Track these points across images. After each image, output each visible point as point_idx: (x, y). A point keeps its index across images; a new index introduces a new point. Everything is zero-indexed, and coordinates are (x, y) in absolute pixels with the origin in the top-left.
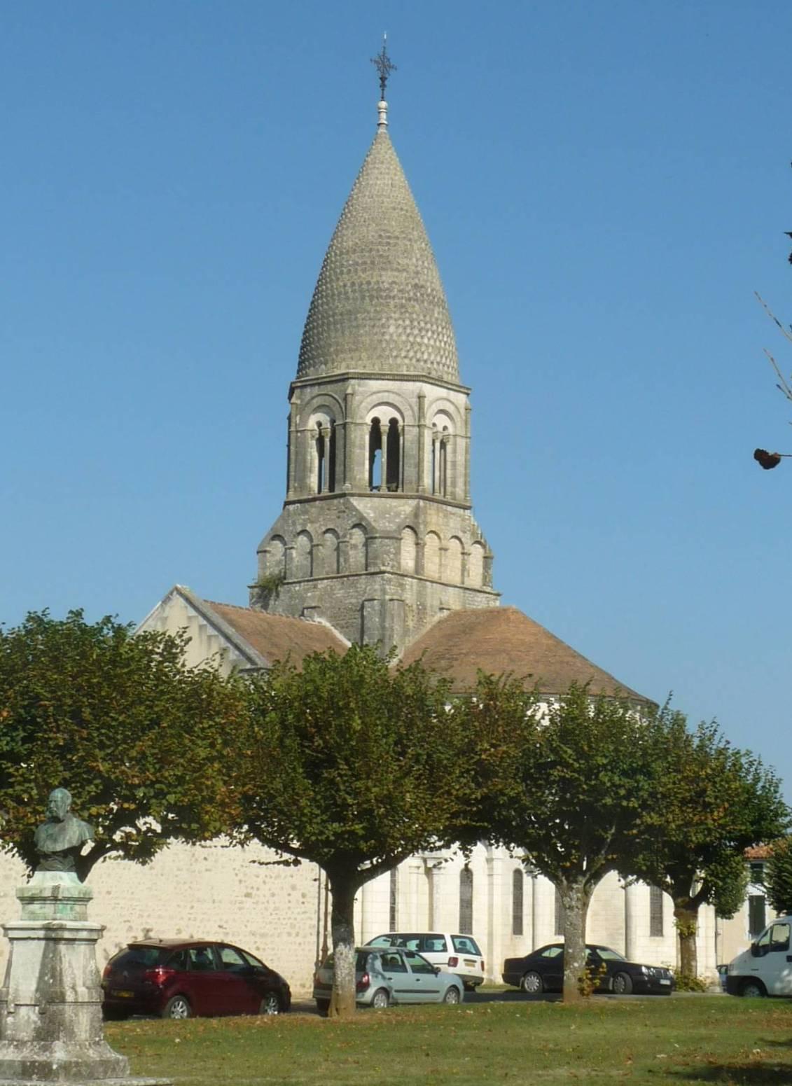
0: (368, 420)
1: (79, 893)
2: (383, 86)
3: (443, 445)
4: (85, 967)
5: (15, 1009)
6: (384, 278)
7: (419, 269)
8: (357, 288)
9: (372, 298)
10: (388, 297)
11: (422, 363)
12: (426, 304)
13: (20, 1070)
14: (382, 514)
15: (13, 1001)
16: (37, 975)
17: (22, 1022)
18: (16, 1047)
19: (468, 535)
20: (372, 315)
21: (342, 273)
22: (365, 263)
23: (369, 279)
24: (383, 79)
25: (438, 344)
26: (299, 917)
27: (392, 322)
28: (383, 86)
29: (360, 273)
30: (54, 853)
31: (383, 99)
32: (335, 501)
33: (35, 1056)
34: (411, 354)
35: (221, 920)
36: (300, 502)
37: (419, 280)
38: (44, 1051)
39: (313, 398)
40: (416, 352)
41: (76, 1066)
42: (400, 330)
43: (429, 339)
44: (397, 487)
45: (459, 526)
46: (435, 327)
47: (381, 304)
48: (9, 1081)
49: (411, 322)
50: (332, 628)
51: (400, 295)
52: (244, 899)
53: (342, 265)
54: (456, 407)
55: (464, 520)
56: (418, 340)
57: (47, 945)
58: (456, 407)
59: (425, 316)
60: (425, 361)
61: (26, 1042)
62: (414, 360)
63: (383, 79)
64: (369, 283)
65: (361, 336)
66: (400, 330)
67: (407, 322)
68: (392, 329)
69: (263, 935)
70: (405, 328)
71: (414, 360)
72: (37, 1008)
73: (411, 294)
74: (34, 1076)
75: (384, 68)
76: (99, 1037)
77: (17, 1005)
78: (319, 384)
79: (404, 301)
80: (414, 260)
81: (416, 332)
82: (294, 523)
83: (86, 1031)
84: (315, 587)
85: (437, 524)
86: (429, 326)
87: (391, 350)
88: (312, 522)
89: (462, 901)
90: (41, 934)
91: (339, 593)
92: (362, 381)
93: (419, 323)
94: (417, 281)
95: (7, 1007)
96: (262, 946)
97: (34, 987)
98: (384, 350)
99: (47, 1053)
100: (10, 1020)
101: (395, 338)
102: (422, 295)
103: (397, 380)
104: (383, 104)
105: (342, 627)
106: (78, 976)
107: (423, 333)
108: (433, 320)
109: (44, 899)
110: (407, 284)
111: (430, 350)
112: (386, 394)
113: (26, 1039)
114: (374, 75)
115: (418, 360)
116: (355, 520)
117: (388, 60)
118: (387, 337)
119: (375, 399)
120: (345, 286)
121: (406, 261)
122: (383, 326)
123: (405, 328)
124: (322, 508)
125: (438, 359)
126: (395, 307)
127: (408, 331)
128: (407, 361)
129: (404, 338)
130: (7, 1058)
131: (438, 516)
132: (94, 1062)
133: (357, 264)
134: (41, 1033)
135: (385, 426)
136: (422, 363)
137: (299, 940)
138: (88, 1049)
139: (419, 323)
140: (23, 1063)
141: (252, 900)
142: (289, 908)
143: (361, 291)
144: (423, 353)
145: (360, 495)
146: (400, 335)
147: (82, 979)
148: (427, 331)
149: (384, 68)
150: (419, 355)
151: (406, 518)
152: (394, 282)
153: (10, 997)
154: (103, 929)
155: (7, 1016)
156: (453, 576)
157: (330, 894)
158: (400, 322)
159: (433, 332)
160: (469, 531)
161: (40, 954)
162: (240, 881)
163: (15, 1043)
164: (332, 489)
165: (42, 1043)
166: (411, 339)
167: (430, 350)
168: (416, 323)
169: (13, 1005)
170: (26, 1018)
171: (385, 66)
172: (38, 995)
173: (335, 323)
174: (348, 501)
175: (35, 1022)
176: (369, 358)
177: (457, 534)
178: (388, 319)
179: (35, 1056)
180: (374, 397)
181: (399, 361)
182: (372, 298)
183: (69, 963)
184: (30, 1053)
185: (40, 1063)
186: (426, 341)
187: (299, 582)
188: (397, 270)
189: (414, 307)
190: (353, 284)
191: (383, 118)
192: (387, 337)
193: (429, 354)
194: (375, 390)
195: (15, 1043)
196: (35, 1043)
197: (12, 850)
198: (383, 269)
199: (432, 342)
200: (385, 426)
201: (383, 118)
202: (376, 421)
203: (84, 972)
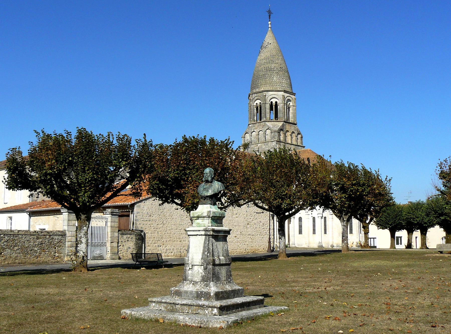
0: (255, 104)
1: (219, 214)
2: (270, 18)
3: (289, 108)
4: (223, 248)
5: (192, 267)
8: (265, 68)
9: (269, 71)
10: (273, 70)
13: (196, 295)
14: (274, 126)
15: (191, 264)
16: (202, 252)
17: (196, 273)
18: (193, 284)
19: (296, 131)
20: (269, 75)
21: (261, 65)
22: (267, 62)
23: (268, 66)
24: (270, 16)
26: (262, 230)
27: (275, 77)
28: (270, 18)
29: (266, 65)
30: (207, 196)
31: (270, 21)
32: (262, 123)
33: (202, 289)
34: (280, 85)
35: (241, 231)
36: (252, 124)
38: (207, 287)
39: (255, 97)
40: (281, 84)
41: (221, 294)
42: (277, 79)
44: (278, 119)
47: (272, 72)
48: (190, 301)
49: (280, 77)
51: (277, 70)
52: (247, 225)
53: (261, 63)
54: (292, 98)
56: (282, 81)
57: (205, 239)
58: (292, 98)
59: (283, 75)
61: (198, 282)
62: (281, 86)
63: (270, 16)
64: (268, 67)
65: (267, 80)
66: (277, 79)
67: (279, 77)
68: (275, 79)
69: (253, 235)
70: (278, 78)
71: (281, 86)
72: (202, 267)
73: (279, 70)
74: (202, 298)
75: (270, 13)
76: (230, 279)
77: (192, 265)
81: (281, 79)
82: (251, 129)
83: (224, 276)
84: (257, 146)
85: (288, 128)
87: (275, 84)
88: (256, 129)
89: (299, 226)
90: (203, 233)
91: (264, 147)
95: (188, 266)
96: (252, 238)
97: (201, 257)
98: (273, 84)
99: (208, 287)
100: (190, 272)
101: (276, 81)
102: (282, 70)
104: (270, 22)
106: (220, 252)
107: (283, 79)
109: (204, 217)
113: (198, 281)
115: (282, 86)
116: (267, 128)
117: (271, 11)
118: (274, 81)
119: (271, 97)
120: (262, 68)
121: (278, 61)
123: (278, 78)
124: (258, 125)
127: (279, 79)
128: (279, 87)
129: (278, 81)
130: (190, 290)
132: (229, 291)
133: (265, 62)
134: (204, 278)
135: (274, 103)
137: (262, 236)
138: (226, 285)
140: (197, 292)
141: (250, 225)
142: (259, 228)
143: (266, 69)
144: (283, 85)
145: (268, 121)
146: (277, 80)
147: (222, 253)
149: (270, 13)
150: (282, 85)
153: (189, 261)
154: (230, 230)
155: (189, 270)
156: (294, 143)
157: (277, 222)
158: (277, 77)
161: (203, 242)
162: (246, 220)
163: (193, 282)
164: (261, 120)
165: (206, 283)
168: (281, 77)
169: (191, 265)
170: (197, 271)
171: (269, 12)
172: (203, 261)
173: (260, 78)
174: (265, 123)
175: (201, 273)
176: (269, 86)
178: (274, 76)
179: (202, 289)
181: (277, 87)
182: (269, 71)
183: (216, 246)
184: (200, 288)
185: (205, 293)
186: (284, 81)
187: (253, 144)
188: (276, 63)
190: (264, 68)
191: (270, 26)
192: (274, 81)
193: (285, 85)
194: (271, 94)
195: (193, 282)
196: (202, 283)
197: (183, 209)
199: (285, 82)
200: (274, 103)
201: (270, 26)
202: (257, 104)
203: (223, 250)
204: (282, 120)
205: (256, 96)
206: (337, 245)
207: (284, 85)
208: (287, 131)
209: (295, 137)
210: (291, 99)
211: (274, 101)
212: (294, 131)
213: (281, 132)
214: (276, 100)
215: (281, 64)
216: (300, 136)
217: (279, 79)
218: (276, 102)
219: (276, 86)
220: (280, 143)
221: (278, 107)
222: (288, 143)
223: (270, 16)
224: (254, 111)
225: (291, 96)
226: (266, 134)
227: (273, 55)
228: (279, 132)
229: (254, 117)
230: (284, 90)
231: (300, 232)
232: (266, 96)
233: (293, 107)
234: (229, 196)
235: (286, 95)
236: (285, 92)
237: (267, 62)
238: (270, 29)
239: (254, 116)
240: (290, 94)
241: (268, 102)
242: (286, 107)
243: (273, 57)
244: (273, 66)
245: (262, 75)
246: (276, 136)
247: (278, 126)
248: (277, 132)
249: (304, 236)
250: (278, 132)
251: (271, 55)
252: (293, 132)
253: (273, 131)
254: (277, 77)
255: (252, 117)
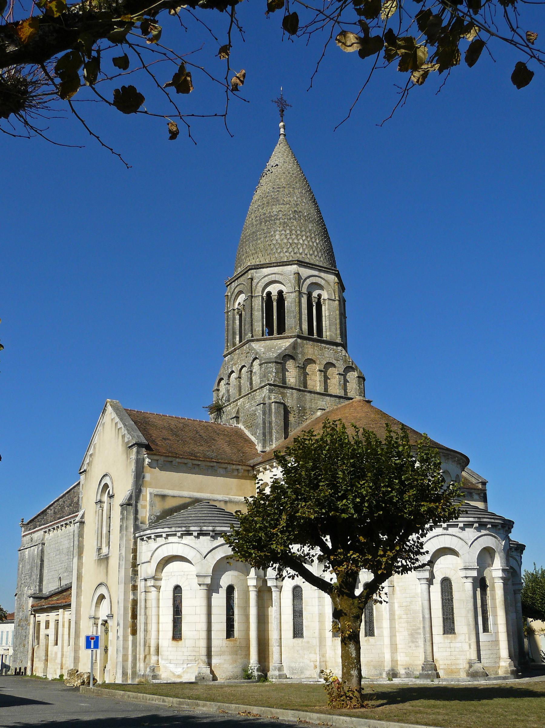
0: (236, 306)
6: (274, 210)
7: (299, 202)
11: (298, 255)
12: (302, 221)
25: (311, 243)
27: (278, 232)
29: (260, 210)
31: (282, 121)
32: (245, 347)
34: (290, 250)
37: (298, 208)
42: (283, 237)
43: (303, 241)
45: (332, 356)
46: (308, 234)
50: (245, 429)
51: (283, 217)
55: (336, 352)
56: (296, 241)
60: (301, 254)
67: (288, 232)
68: (277, 237)
71: (292, 253)
73: (292, 216)
78: (237, 279)
79: (286, 220)
80: (295, 198)
81: (294, 237)
86: (304, 233)
92: (258, 270)
93: (296, 232)
94: (296, 209)
101: (279, 241)
103: (280, 266)
105: (249, 428)
107: (299, 237)
108: (307, 230)
110: (289, 211)
111: (305, 247)
112: (274, 275)
114: (276, 109)
115: (295, 253)
116: (253, 356)
118: (274, 242)
119: (267, 280)
121: (288, 199)
122: (272, 236)
125: (311, 252)
126: (280, 224)
128: (287, 254)
129: (285, 241)
131: (314, 348)
135: (274, 294)
136: (298, 255)
139: (296, 232)
145: (258, 340)
148: (302, 236)
151: (285, 349)
152: (280, 211)
158: (283, 232)
159: (307, 237)
160: (342, 360)
166: (290, 241)
167: (305, 247)
168: (294, 232)
177: (331, 362)
180: (266, 278)
181: (282, 255)
186: (301, 241)
188: (283, 204)
189: (292, 223)
191: (282, 131)
192: (274, 242)
193: (304, 250)
198: (273, 205)
199: (306, 242)
200: (274, 294)
201: (282, 131)
204: (293, 332)
205: (237, 286)
206: (407, 670)
207: (301, 251)
208: (311, 361)
209: (337, 376)
210: (322, 282)
211: (274, 289)
212: (334, 362)
213: (290, 364)
214: (277, 287)
215: (297, 205)
216: (352, 376)
217: (288, 237)
218: (280, 293)
219: (280, 252)
220: (282, 390)
221: (286, 302)
222: (310, 392)
223: (283, 111)
224: (234, 322)
225: (323, 275)
226: (254, 371)
227: (279, 188)
228: (280, 363)
229: (234, 338)
230: (298, 261)
231: (298, 632)
232: (255, 281)
233: (331, 302)
234: (234, 546)
235: (305, 272)
236: (301, 263)
237: (263, 204)
238: (282, 137)
239: (234, 334)
240: (320, 271)
241: (258, 292)
242: (304, 300)
243: (278, 191)
244: (275, 209)
245: (249, 236)
246: (271, 372)
247: (280, 348)
248: (273, 362)
249: (308, 642)
250: (276, 362)
251: (274, 188)
252: (330, 365)
253: (265, 359)
254: (283, 232)
255: (230, 337)
